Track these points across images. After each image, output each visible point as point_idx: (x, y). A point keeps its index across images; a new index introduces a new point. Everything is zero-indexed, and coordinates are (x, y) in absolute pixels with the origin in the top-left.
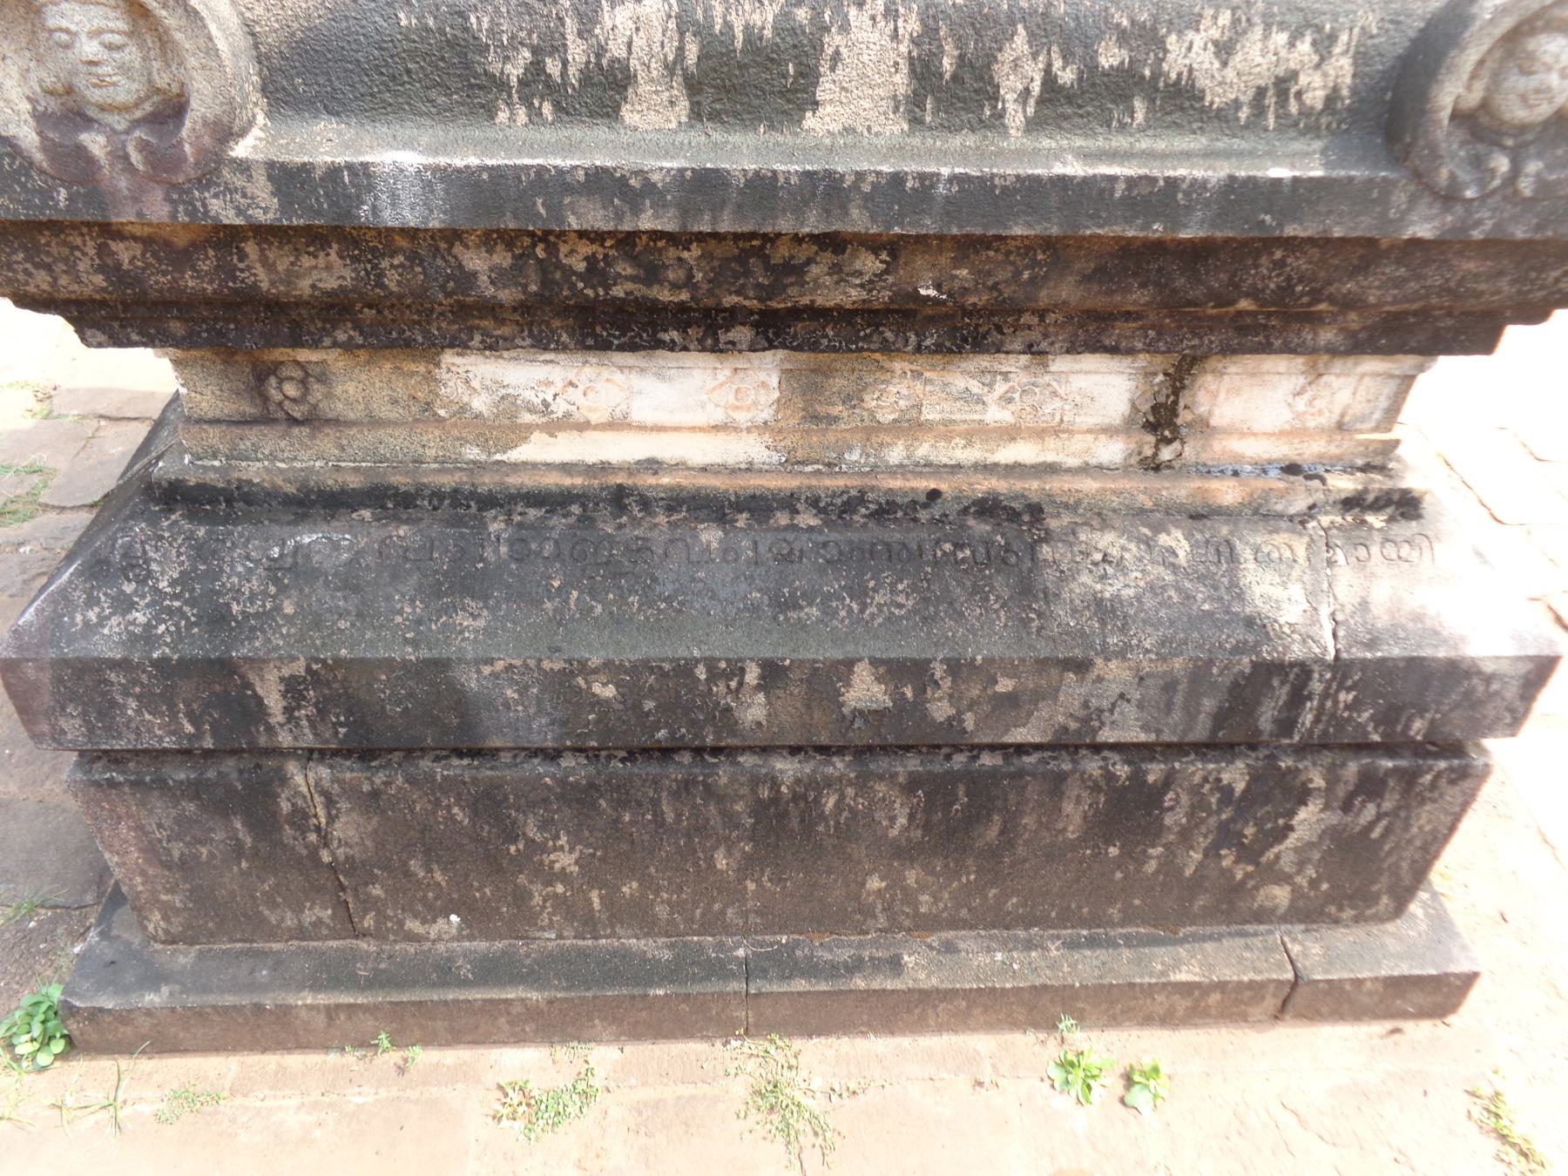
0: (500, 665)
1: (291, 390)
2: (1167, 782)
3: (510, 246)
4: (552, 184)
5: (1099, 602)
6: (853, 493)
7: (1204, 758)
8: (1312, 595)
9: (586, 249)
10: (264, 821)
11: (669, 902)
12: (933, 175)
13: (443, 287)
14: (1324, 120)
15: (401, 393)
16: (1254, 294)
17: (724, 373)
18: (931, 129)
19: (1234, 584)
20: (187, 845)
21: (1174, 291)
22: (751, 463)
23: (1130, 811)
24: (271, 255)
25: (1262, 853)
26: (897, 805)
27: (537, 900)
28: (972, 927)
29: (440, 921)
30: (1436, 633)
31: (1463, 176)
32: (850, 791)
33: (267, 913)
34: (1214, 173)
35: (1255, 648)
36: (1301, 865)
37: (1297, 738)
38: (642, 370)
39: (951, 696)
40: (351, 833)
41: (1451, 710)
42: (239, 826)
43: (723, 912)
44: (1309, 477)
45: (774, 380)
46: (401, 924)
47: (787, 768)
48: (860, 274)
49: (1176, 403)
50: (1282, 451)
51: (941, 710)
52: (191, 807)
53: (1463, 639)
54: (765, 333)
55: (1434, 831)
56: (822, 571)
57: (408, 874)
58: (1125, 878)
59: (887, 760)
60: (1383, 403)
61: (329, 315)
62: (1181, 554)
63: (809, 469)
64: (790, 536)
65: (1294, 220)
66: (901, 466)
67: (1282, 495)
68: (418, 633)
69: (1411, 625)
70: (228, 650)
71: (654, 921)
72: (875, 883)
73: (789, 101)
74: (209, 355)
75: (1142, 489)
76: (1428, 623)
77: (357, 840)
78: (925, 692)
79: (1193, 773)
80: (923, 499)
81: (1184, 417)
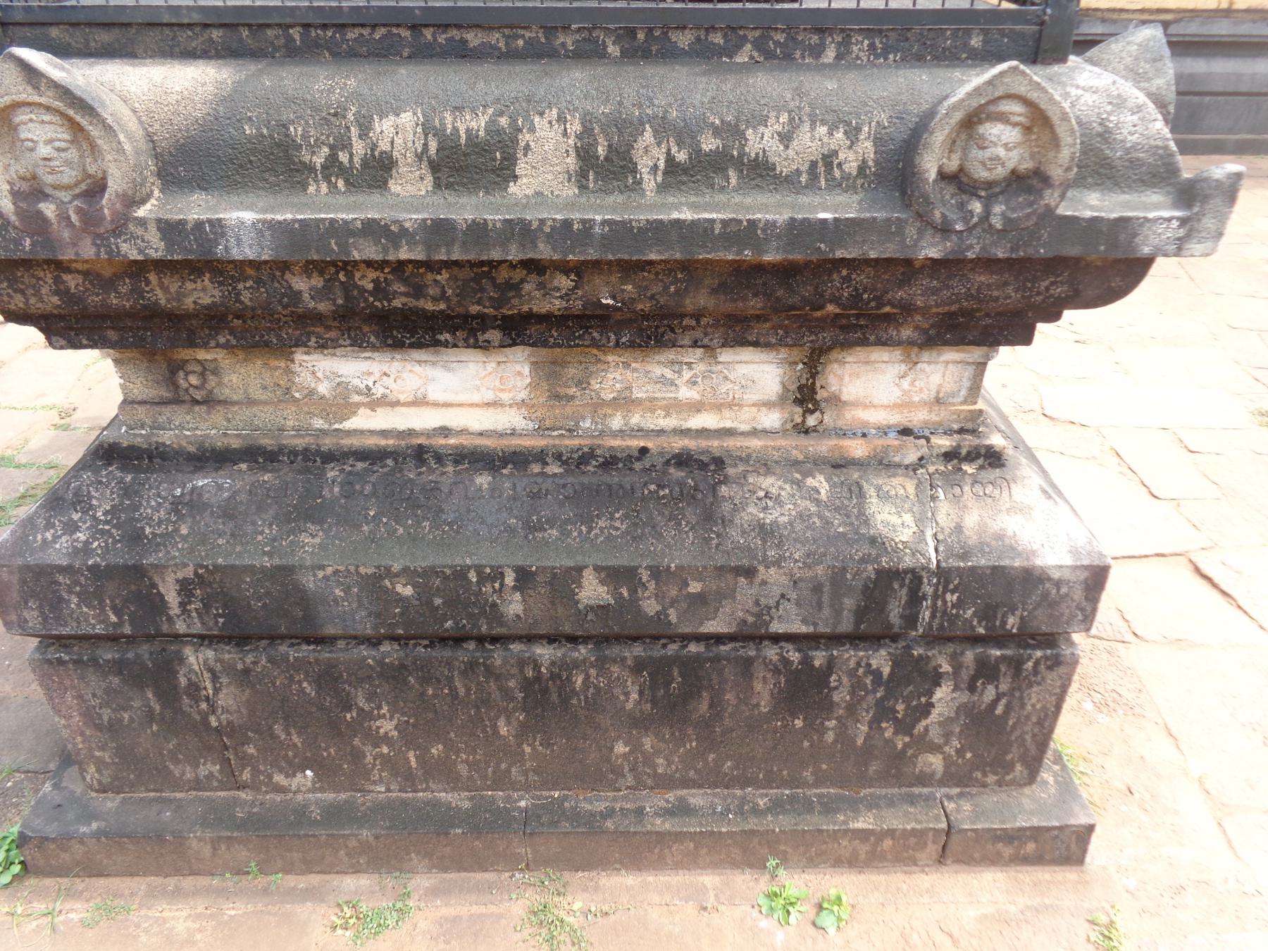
0: (329, 570)
1: (194, 380)
2: (830, 666)
3: (321, 273)
4: (340, 230)
5: (761, 526)
6: (586, 450)
7: (856, 648)
8: (920, 521)
9: (372, 274)
10: (168, 694)
11: (467, 762)
12: (590, 220)
13: (280, 302)
14: (859, 182)
15: (269, 381)
16: (835, 300)
17: (491, 366)
18: (593, 192)
19: (861, 513)
20: (114, 711)
21: (777, 298)
22: (514, 429)
23: (805, 690)
24: (166, 282)
25: (913, 727)
26: (629, 683)
27: (369, 759)
28: (700, 786)
29: (299, 775)
30: (1013, 549)
31: (951, 216)
32: (593, 672)
33: (172, 767)
34: (781, 217)
35: (876, 559)
36: (947, 736)
37: (921, 631)
38: (434, 364)
39: (657, 596)
40: (231, 702)
41: (1034, 609)
42: (150, 696)
43: (508, 771)
44: (918, 438)
45: (526, 370)
46: (270, 777)
47: (544, 652)
48: (559, 289)
49: (813, 383)
50: (896, 418)
51: (650, 607)
52: (116, 681)
53: (1034, 552)
54: (510, 334)
55: (1044, 708)
56: (561, 504)
57: (273, 736)
58: (811, 746)
59: (618, 648)
60: (966, 383)
61: (212, 323)
62: (823, 492)
63: (555, 433)
64: (540, 480)
65: (841, 247)
66: (621, 431)
67: (898, 449)
68: (273, 547)
69: (993, 543)
70: (141, 559)
71: (458, 778)
72: (620, 748)
73: (498, 176)
74: (138, 356)
75: (795, 446)
76: (1007, 541)
77: (235, 708)
78: (636, 592)
79: (848, 659)
80: (636, 454)
81: (821, 394)
